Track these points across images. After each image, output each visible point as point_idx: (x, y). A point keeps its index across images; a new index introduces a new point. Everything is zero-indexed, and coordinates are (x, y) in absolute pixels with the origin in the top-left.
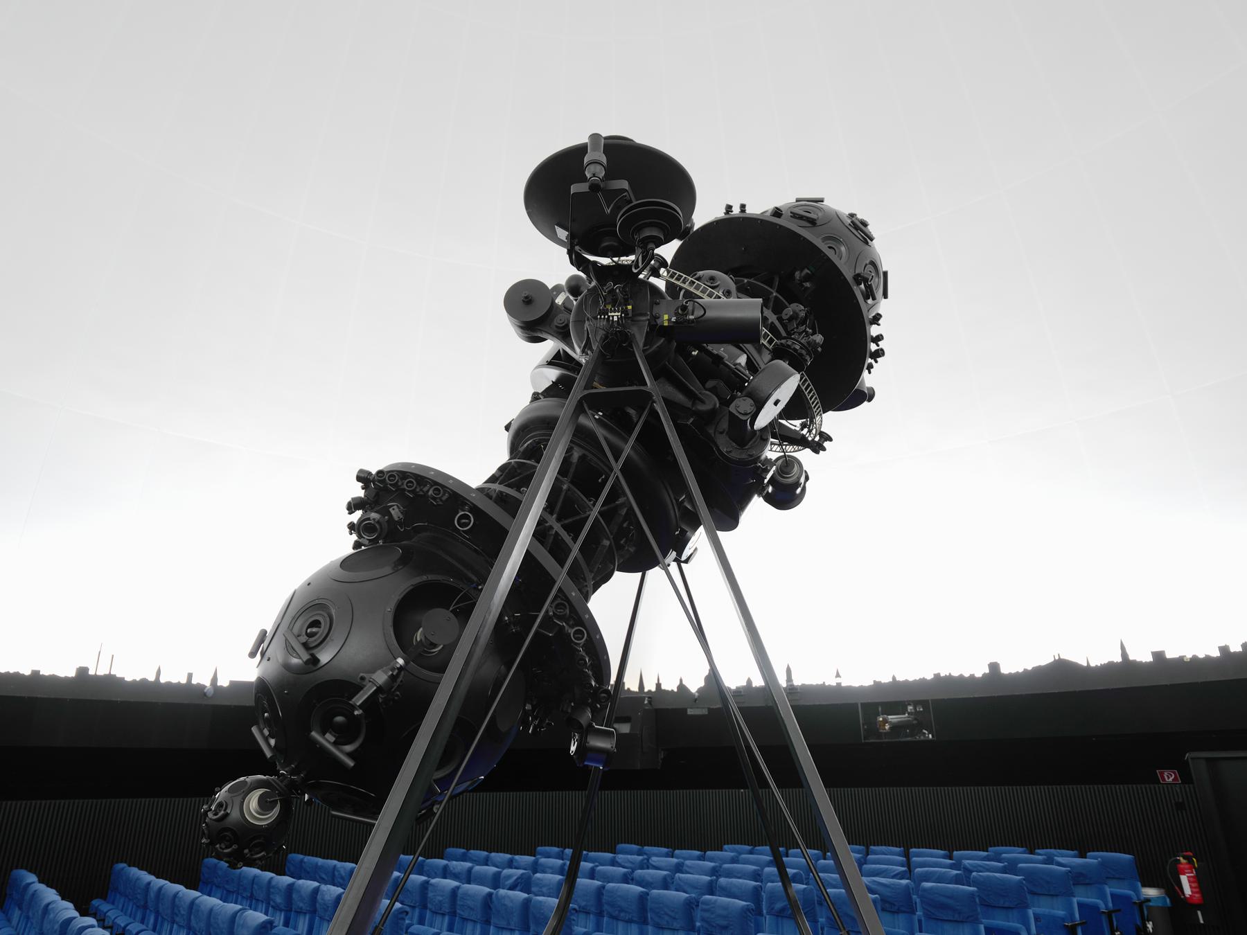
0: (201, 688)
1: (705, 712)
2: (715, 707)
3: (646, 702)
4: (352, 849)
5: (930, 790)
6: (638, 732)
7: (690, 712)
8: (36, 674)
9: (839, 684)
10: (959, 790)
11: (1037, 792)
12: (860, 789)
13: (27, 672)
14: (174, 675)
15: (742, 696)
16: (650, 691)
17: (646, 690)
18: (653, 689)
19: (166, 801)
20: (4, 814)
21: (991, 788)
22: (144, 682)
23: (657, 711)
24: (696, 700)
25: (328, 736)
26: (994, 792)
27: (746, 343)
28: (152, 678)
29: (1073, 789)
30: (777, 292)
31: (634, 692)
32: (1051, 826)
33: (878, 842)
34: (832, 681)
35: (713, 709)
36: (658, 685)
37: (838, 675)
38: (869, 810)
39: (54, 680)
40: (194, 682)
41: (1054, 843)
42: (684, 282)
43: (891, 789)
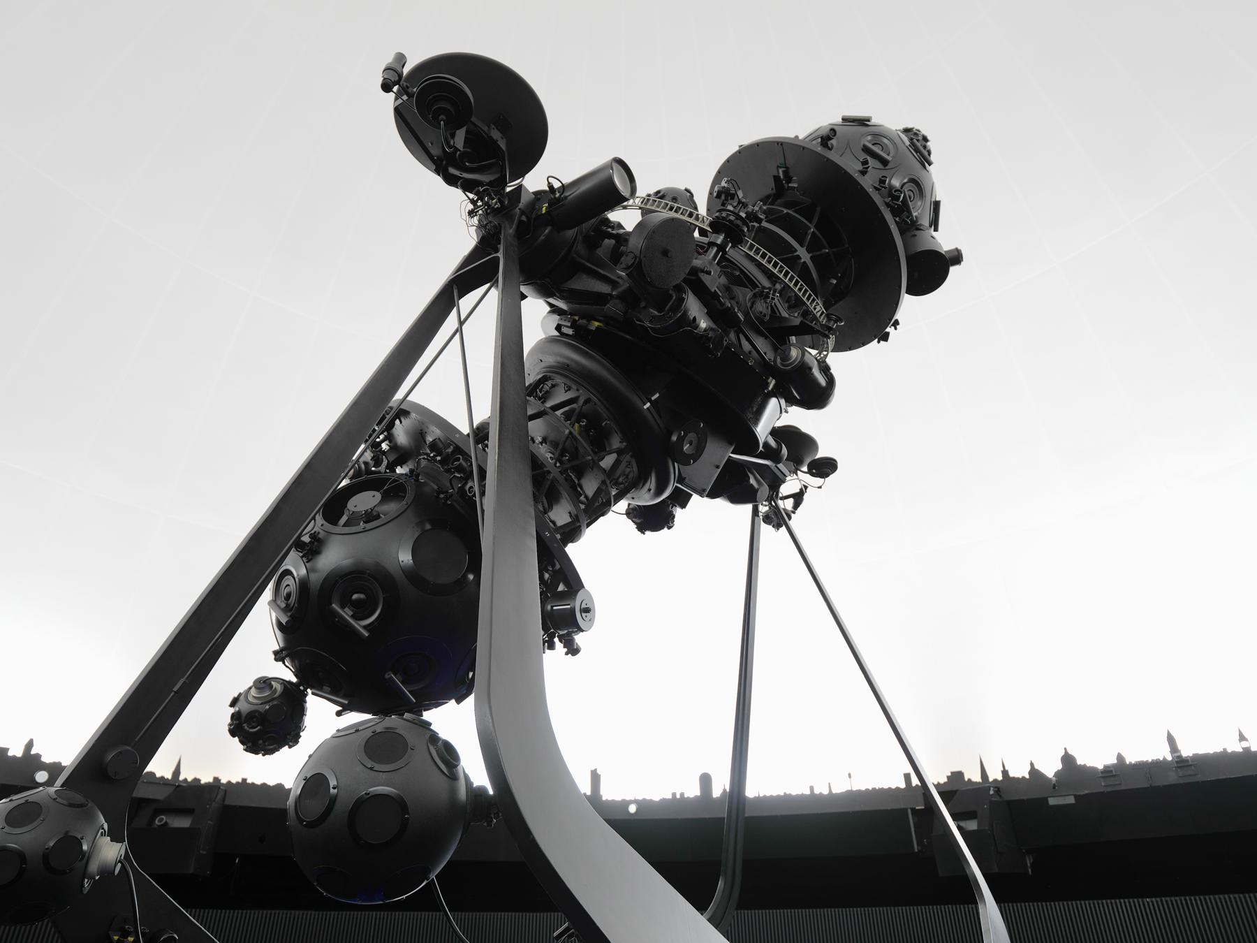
1: (1071, 800)
2: (1082, 793)
3: (992, 792)
6: (987, 828)
7: (1052, 801)
9: (1247, 750)
11: (861, 914)
15: (1115, 776)
16: (995, 781)
17: (991, 780)
18: (1000, 778)
19: (361, 915)
20: (3, 932)
21: (904, 908)
22: (679, 803)
23: (1010, 804)
24: (1054, 786)
25: (347, 610)
26: (1231, 902)
34: (1235, 747)
36: (1005, 773)
37: (1242, 738)
40: (686, 796)
43: (877, 909)
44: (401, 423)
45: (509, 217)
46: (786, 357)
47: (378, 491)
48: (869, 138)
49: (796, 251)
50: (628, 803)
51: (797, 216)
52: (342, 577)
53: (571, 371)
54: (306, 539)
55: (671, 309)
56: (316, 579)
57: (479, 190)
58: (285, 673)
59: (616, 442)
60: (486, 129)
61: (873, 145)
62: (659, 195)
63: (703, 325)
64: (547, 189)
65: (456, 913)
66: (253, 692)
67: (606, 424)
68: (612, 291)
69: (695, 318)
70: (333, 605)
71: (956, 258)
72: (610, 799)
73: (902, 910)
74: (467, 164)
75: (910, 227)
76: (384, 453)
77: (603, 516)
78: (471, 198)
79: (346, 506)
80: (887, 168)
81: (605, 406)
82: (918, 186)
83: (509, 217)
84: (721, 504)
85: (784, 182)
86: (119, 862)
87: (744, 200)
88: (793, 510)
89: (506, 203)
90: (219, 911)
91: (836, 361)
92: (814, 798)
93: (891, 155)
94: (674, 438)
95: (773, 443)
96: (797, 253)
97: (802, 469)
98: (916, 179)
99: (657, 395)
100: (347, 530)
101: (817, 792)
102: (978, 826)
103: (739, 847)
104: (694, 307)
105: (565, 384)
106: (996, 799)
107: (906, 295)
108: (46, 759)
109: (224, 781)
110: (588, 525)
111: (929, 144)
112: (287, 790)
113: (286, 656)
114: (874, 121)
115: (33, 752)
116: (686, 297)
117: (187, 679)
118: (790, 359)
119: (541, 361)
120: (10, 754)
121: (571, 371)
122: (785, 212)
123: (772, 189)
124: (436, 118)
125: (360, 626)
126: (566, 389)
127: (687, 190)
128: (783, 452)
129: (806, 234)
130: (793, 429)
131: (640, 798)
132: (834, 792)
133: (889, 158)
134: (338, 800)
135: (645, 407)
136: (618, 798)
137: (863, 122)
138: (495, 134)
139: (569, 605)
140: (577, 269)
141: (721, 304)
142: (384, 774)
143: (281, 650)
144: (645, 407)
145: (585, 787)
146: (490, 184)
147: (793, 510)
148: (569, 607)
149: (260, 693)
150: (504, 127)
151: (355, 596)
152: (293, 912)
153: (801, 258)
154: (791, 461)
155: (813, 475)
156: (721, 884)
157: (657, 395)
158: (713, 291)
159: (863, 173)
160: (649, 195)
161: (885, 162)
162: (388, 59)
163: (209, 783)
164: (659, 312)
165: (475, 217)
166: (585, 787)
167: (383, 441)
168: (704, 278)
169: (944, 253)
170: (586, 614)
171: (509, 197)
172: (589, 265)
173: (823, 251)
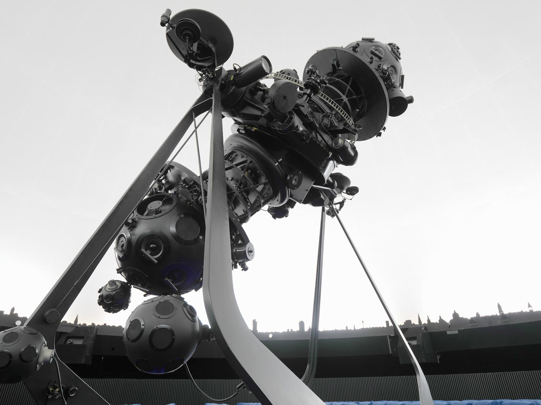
1: (457, 332)
2: (461, 329)
3: (423, 329)
4: (442, 396)
5: (373, 378)
7: (448, 333)
9: (531, 311)
10: (342, 379)
12: (368, 378)
15: (475, 322)
16: (425, 324)
18: (427, 323)
24: (449, 326)
25: (148, 251)
26: (523, 374)
30: (350, 86)
31: (416, 325)
33: (383, 399)
34: (527, 310)
35: (460, 330)
36: (429, 321)
37: (529, 306)
38: (10, 398)
41: (456, 398)
44: (170, 171)
46: (336, 143)
48: (374, 47)
49: (341, 97)
52: (146, 237)
54: (130, 221)
55: (287, 122)
58: (122, 278)
59: (263, 180)
60: (206, 43)
61: (375, 50)
62: (282, 72)
65: (196, 380)
66: (108, 286)
72: (261, 332)
73: (451, 376)
74: (198, 58)
75: (391, 86)
76: (163, 184)
80: (381, 60)
82: (394, 68)
84: (308, 206)
86: (52, 357)
89: (215, 75)
91: (358, 145)
92: (347, 331)
94: (288, 178)
95: (331, 180)
99: (281, 159)
100: (148, 217)
101: (349, 329)
106: (425, 332)
107: (389, 116)
108: (20, 316)
109: (96, 325)
110: (251, 215)
111: (399, 50)
114: (376, 40)
115: (14, 313)
118: (339, 144)
119: (231, 145)
120: (5, 313)
123: (331, 70)
124: (184, 38)
125: (154, 258)
128: (335, 184)
133: (382, 56)
135: (276, 165)
137: (371, 40)
138: (211, 45)
139: (243, 249)
140: (246, 104)
141: (309, 120)
143: (120, 269)
144: (276, 165)
146: (209, 67)
149: (111, 287)
150: (214, 42)
151: (151, 246)
156: (308, 367)
157: (281, 159)
158: (305, 114)
159: (371, 63)
160: (278, 72)
161: (380, 58)
162: (163, 12)
163: (90, 325)
164: (282, 123)
167: (163, 179)
169: (405, 98)
170: (250, 253)
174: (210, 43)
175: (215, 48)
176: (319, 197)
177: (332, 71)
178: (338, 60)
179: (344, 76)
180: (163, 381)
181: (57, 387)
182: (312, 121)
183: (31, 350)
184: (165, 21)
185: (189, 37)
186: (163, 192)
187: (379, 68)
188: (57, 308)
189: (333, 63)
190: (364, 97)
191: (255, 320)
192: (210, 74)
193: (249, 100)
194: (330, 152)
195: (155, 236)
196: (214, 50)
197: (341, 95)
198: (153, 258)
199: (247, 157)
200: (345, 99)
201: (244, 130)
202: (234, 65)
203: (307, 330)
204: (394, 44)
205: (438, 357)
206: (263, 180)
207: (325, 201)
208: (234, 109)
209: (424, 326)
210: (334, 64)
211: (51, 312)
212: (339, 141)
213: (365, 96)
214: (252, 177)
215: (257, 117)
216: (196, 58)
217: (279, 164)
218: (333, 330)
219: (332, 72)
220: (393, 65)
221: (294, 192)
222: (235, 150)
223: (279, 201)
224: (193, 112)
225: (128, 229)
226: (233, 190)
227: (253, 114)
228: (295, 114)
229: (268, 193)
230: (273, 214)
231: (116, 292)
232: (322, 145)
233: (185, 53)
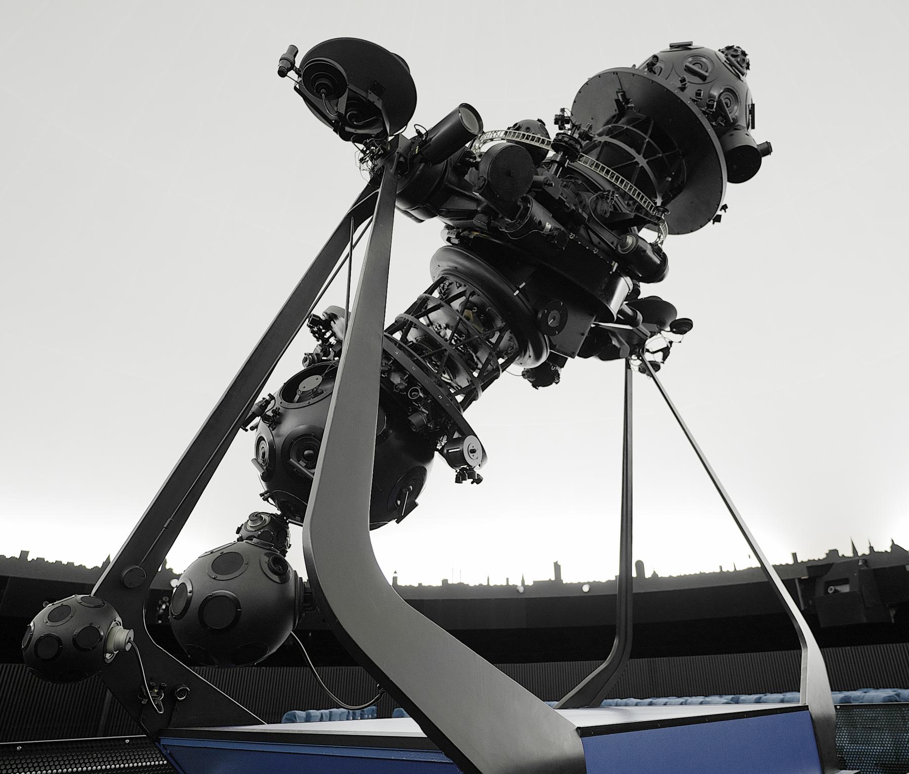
0: (515, 587)
3: (860, 563)
8: (594, 581)
13: (416, 585)
14: (498, 581)
16: (864, 555)
18: (867, 552)
25: (301, 462)
27: (357, 142)
28: (485, 583)
29: (779, 654)
30: (650, 137)
32: (256, 682)
36: (871, 548)
39: (430, 588)
40: (511, 583)
42: (524, 135)
44: (335, 323)
45: (391, 161)
46: (623, 244)
47: (321, 375)
48: (690, 59)
49: (635, 158)
50: (582, 584)
51: (634, 129)
52: (295, 439)
53: (459, 272)
54: (270, 413)
55: (520, 217)
56: (279, 441)
57: (366, 142)
58: (272, 509)
59: (499, 324)
60: (364, 94)
61: (694, 65)
62: (516, 127)
63: (548, 226)
64: (417, 135)
65: (319, 668)
66: (250, 523)
67: (489, 309)
68: (477, 207)
69: (540, 222)
70: (291, 460)
71: (767, 149)
72: (569, 582)
74: (355, 123)
75: (728, 127)
76: (331, 346)
77: (497, 378)
78: (361, 149)
79: (298, 388)
80: (706, 82)
81: (487, 297)
82: (733, 94)
83: (391, 161)
84: (594, 361)
85: (624, 104)
86: (129, 642)
87: (577, 124)
88: (662, 361)
89: (389, 148)
90: (299, 668)
91: (673, 245)
92: (722, 575)
93: (709, 70)
94: (540, 316)
95: (629, 311)
96: (635, 160)
97: (666, 330)
98: (731, 88)
99: (524, 284)
100: (297, 405)
101: (724, 570)
102: (851, 589)
103: (630, 611)
104: (538, 212)
105: (457, 282)
106: (865, 568)
107: (728, 184)
110: (484, 388)
111: (747, 57)
112: (398, 586)
113: (268, 497)
114: (695, 44)
116: (531, 206)
117: (172, 518)
118: (627, 245)
119: (439, 266)
121: (459, 272)
122: (625, 128)
123: (616, 110)
124: (318, 92)
126: (458, 285)
127: (539, 120)
128: (638, 318)
129: (643, 143)
130: (658, 299)
131: (591, 581)
132: (737, 569)
133: (707, 74)
134: (193, 599)
135: (515, 294)
136: (575, 581)
137: (686, 47)
138: (372, 97)
139: (459, 448)
140: (450, 193)
141: (568, 208)
142: (224, 581)
143: (266, 493)
144: (515, 294)
145: (391, 583)
146: (377, 136)
147: (662, 361)
148: (459, 450)
149: (254, 523)
150: (378, 89)
151: (306, 452)
152: (352, 667)
153: (639, 164)
154: (656, 323)
155: (674, 332)
156: (616, 642)
157: (524, 284)
158: (557, 198)
159: (683, 89)
160: (509, 128)
161: (704, 78)
162: (284, 50)
164: (511, 220)
165: (365, 164)
166: (391, 583)
167: (330, 337)
168: (548, 189)
169: (756, 147)
170: (473, 454)
171: (390, 144)
172: (458, 189)
173: (658, 155)
174: (370, 93)
175: (381, 101)
176: (609, 345)
177: (617, 112)
178: (624, 92)
179: (639, 119)
180: (330, 671)
181: (154, 686)
182: (573, 209)
183: (91, 631)
184: (287, 68)
185: (326, 90)
186: (332, 359)
187: (698, 97)
188: (140, 564)
189: (617, 98)
190: (680, 154)
191: (557, 562)
192: (376, 148)
193: (453, 185)
194: (614, 262)
195: (310, 435)
196: (379, 104)
197: (632, 156)
198: (311, 473)
199: (465, 286)
200: (642, 161)
201: (457, 237)
202: (416, 126)
203: (650, 576)
204: (737, 47)
205: (892, 613)
206: (499, 324)
207: (621, 350)
208: (429, 205)
209: (862, 558)
210: (619, 100)
211: (132, 570)
212: (627, 240)
213: (680, 152)
214: (480, 319)
215: (471, 214)
216: (350, 123)
217: (522, 294)
218: (696, 574)
219: (618, 114)
220: (728, 87)
221: (557, 339)
222: (447, 275)
223: (532, 358)
224: (352, 218)
225: (269, 427)
226: (443, 347)
227: (464, 208)
228: (533, 199)
229: (512, 345)
230: (532, 380)
231: (262, 531)
232: (596, 251)
233: (332, 116)
